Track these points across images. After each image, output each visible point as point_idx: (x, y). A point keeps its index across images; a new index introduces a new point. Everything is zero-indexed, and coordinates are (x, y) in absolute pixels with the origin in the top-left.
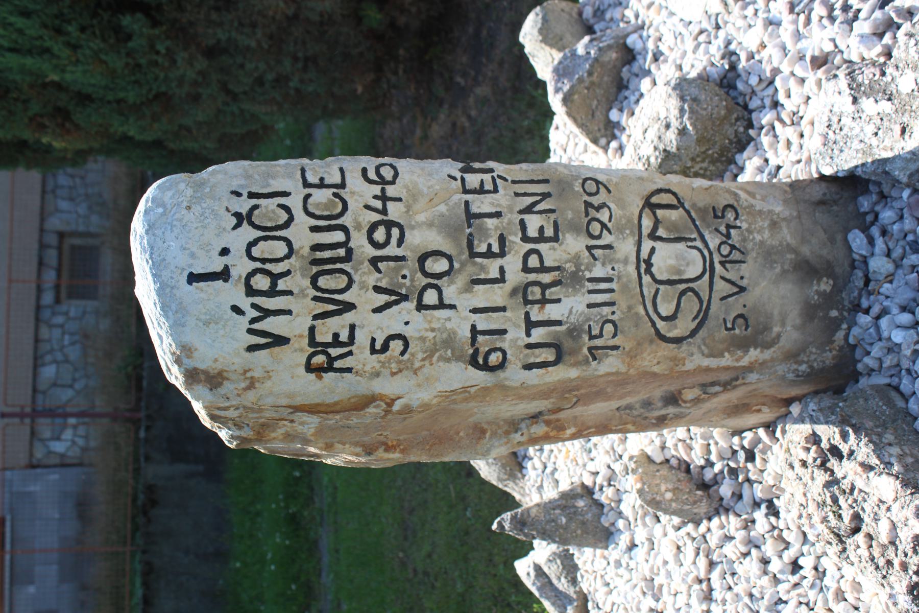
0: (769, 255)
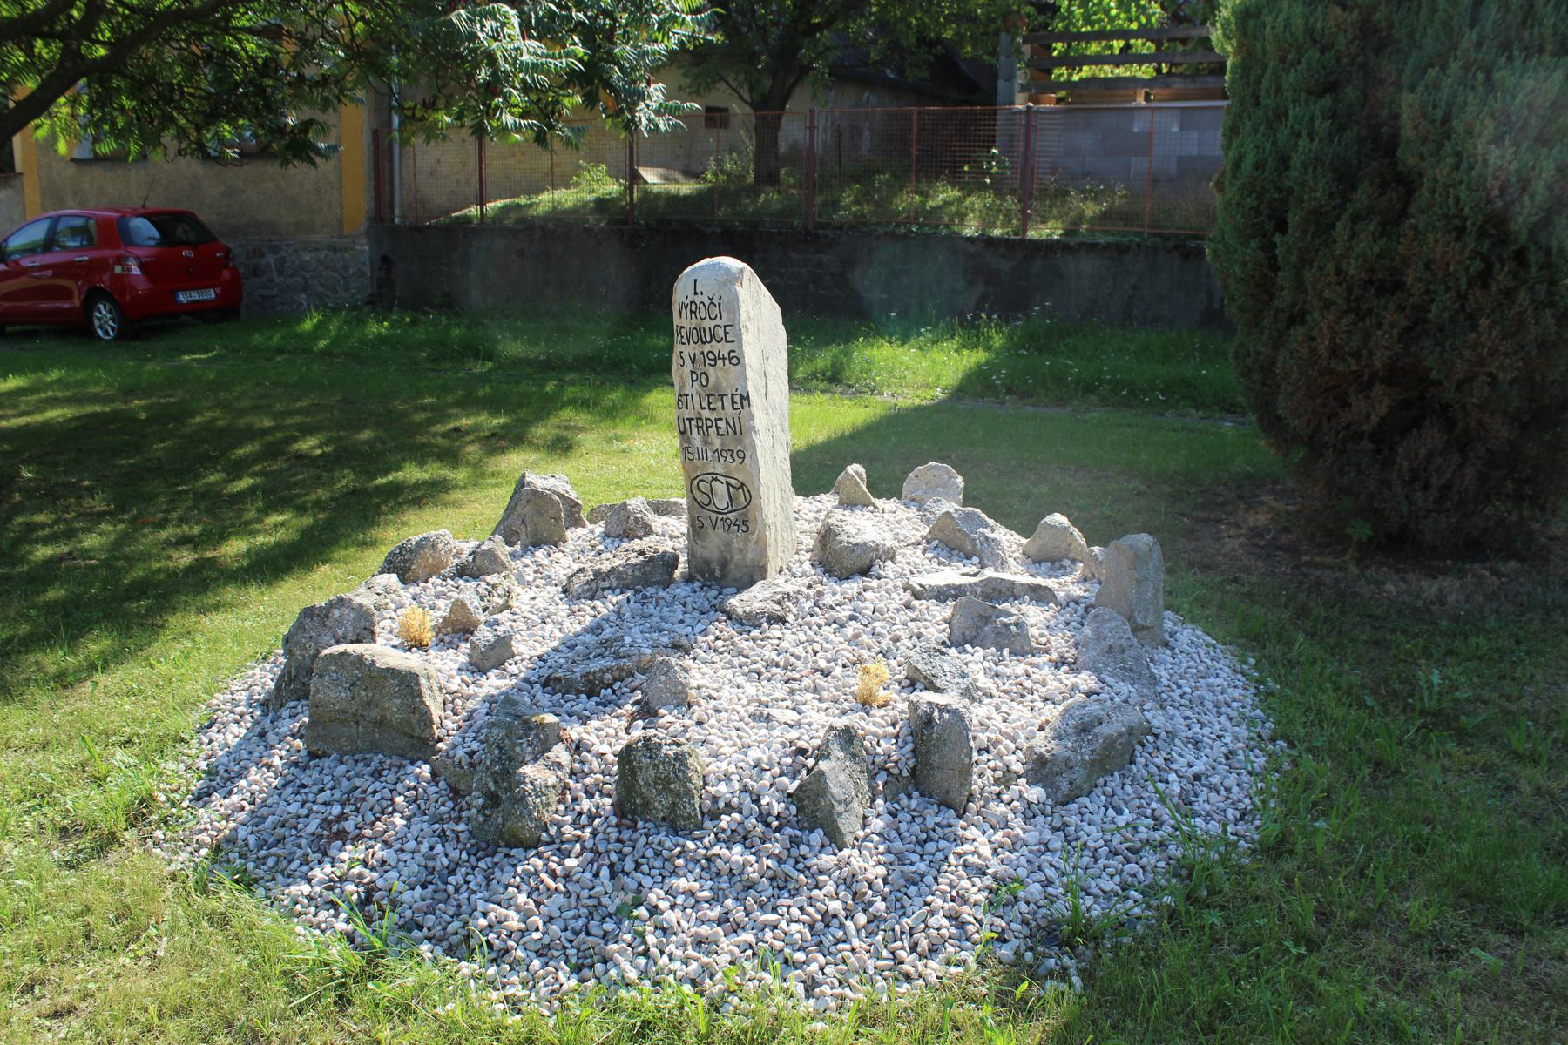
0: (728, 545)
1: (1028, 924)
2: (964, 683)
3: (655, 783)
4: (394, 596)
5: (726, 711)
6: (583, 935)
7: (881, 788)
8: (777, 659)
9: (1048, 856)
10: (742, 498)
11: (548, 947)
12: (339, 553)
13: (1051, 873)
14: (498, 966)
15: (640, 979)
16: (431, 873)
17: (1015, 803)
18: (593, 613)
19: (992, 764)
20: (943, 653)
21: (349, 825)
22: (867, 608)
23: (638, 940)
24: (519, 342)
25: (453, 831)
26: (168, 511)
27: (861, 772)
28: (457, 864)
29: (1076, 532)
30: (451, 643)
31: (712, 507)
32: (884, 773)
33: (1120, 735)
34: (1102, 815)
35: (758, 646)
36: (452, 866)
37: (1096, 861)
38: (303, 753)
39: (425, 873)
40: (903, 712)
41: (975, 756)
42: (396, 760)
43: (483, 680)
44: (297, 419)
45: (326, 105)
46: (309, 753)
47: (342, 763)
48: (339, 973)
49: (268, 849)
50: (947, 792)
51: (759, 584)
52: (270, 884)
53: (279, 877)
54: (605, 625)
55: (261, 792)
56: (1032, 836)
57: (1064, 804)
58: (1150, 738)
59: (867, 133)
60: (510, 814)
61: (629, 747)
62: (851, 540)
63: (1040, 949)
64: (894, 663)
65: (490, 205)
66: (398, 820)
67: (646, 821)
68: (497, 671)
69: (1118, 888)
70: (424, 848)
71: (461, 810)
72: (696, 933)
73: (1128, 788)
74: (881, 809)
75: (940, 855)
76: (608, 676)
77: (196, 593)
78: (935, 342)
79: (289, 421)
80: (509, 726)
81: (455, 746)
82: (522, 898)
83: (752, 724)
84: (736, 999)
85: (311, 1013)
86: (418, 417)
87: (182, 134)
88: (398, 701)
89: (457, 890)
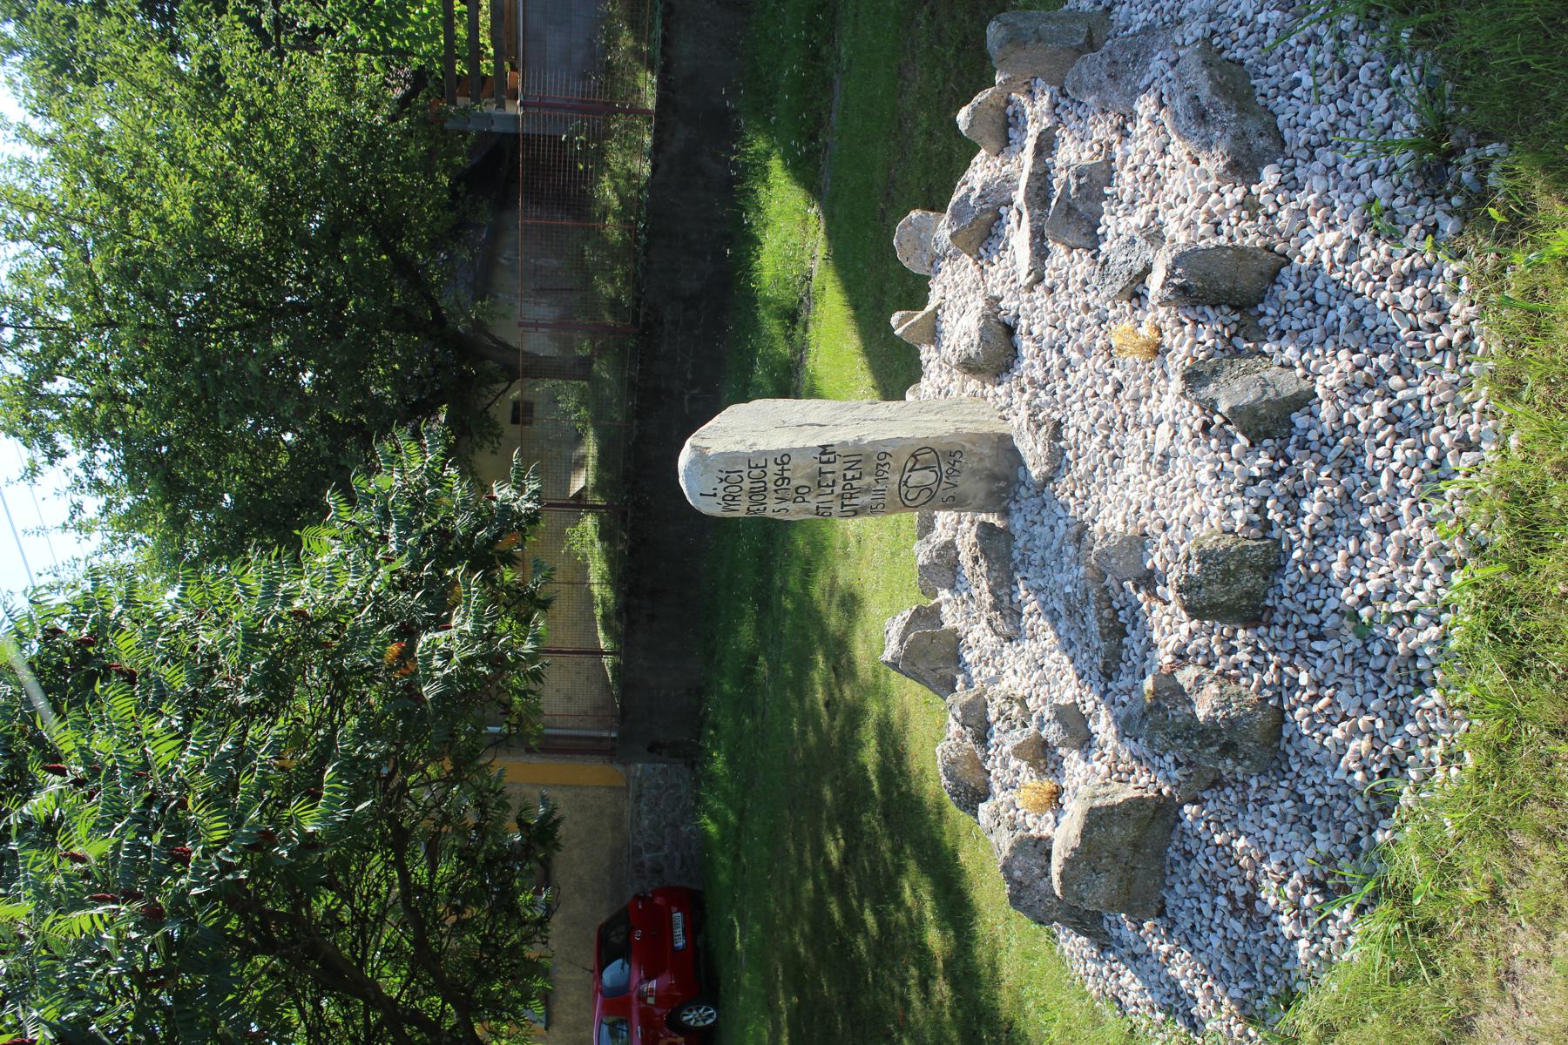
0: (974, 472)
1: (1418, 198)
2: (1140, 241)
3: (1227, 584)
4: (1002, 809)
5: (1154, 498)
6: (1384, 677)
7: (1251, 345)
8: (1100, 437)
9: (1343, 168)
10: (927, 456)
11: (1393, 713)
12: (948, 840)
13: (1362, 167)
14: (1407, 766)
15: (1438, 624)
16: (1300, 819)
17: (1279, 199)
18: (1035, 617)
19: (1233, 221)
20: (1106, 261)
21: (1240, 892)
22: (1051, 335)
23: (1395, 620)
24: (739, 628)
25: (1258, 791)
26: (893, 996)
27: (1232, 365)
28: (1293, 791)
29: (979, 98)
30: (1056, 763)
31: (934, 487)
32: (1236, 340)
33: (1211, 76)
34: (1299, 103)
35: (1084, 454)
36: (1295, 797)
37: (1351, 113)
38: (1158, 922)
39: (1298, 825)
40: (1168, 312)
41: (1223, 240)
42: (1175, 837)
43: (1100, 738)
44: (807, 856)
45: (503, 805)
46: (1158, 916)
47: (1172, 887)
48: (1398, 926)
49: (1255, 971)
50: (1261, 274)
51: (1017, 444)
52: (1294, 976)
53: (1287, 966)
54: (1050, 606)
55: (1194, 968)
56: (1318, 184)
57: (1284, 144)
58: (1215, 41)
59: (541, 262)
60: (1246, 735)
61: (1186, 609)
62: (975, 343)
63: (1449, 187)
64: (1112, 313)
65: (602, 645)
66: (1240, 843)
67: (1266, 596)
68: (1091, 722)
69: (1387, 92)
70: (1272, 823)
71: (1236, 780)
72: (1394, 559)
73: (1271, 70)
74: (1274, 347)
75: (1331, 288)
76: (1106, 613)
77: (978, 986)
78: (759, 210)
79: (809, 863)
80: (1153, 726)
81: (1168, 778)
82: (1337, 733)
83: (1170, 473)
84: (1474, 525)
85: (1438, 961)
86: (812, 738)
87: (526, 939)
88: (1116, 829)
89: (1321, 796)
